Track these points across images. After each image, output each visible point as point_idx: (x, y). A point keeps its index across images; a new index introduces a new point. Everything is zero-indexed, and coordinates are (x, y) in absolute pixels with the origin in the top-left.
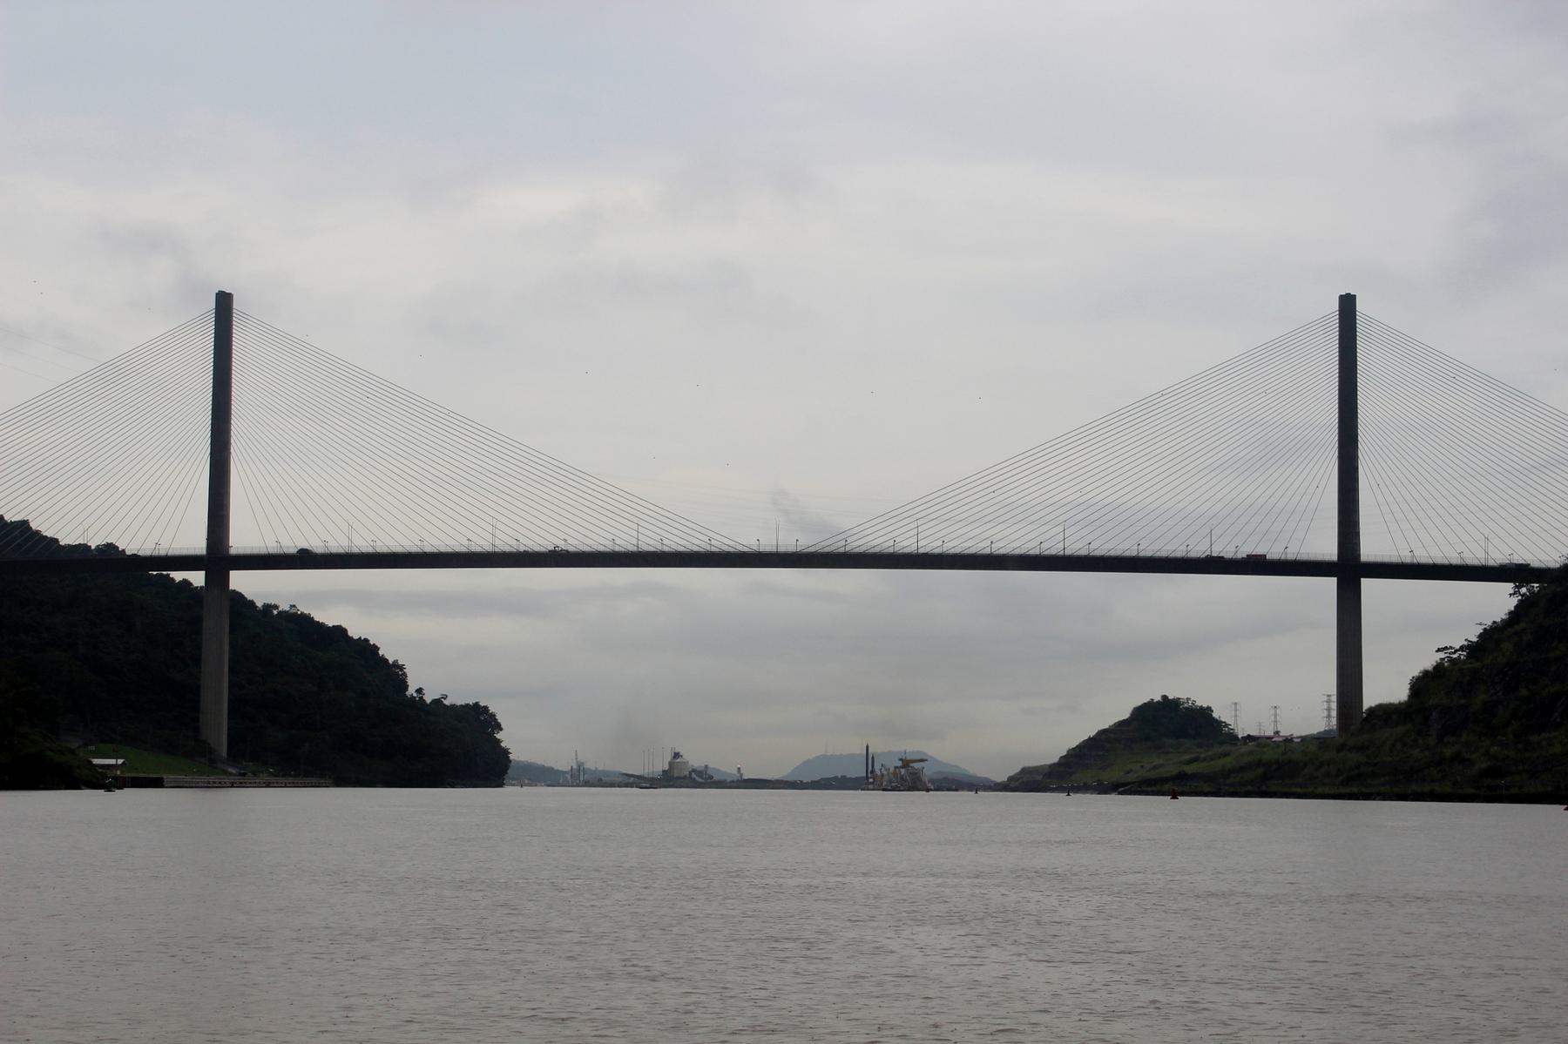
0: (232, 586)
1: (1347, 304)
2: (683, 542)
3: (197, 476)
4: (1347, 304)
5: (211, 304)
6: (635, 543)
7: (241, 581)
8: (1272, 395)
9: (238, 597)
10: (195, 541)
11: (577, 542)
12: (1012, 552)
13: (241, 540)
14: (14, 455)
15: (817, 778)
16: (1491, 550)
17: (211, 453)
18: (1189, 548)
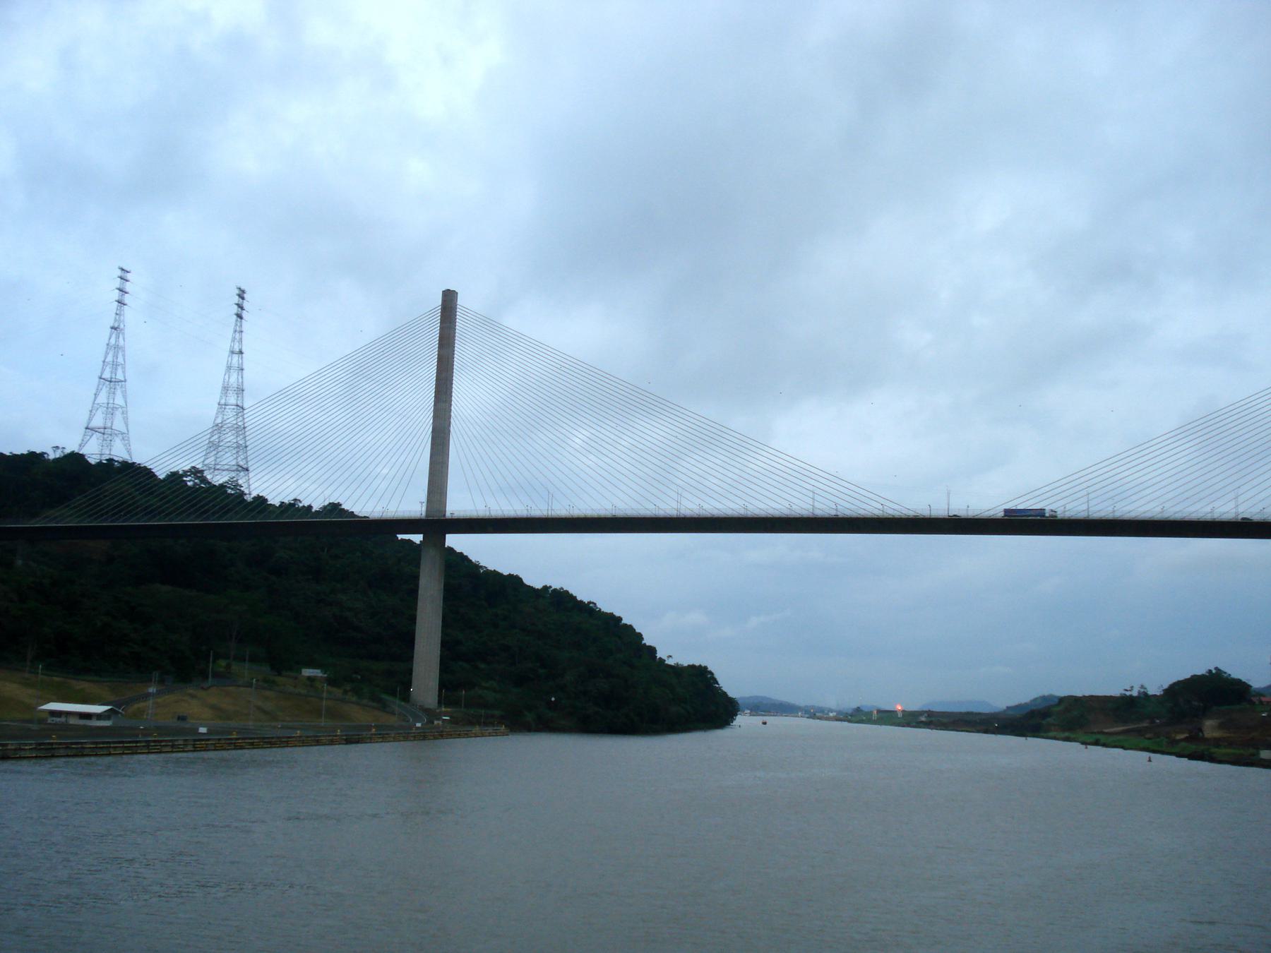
0: (399, 538)
1: (449, 298)
2: (864, 506)
3: (421, 449)
4: (449, 298)
5: (438, 301)
6: (834, 507)
7: (456, 541)
8: (562, 373)
9: (451, 550)
10: (413, 505)
11: (781, 506)
12: (1205, 517)
13: (458, 504)
14: (1241, 433)
15: (914, 706)
16: (685, 502)
17: (432, 432)
18: (1115, 509)
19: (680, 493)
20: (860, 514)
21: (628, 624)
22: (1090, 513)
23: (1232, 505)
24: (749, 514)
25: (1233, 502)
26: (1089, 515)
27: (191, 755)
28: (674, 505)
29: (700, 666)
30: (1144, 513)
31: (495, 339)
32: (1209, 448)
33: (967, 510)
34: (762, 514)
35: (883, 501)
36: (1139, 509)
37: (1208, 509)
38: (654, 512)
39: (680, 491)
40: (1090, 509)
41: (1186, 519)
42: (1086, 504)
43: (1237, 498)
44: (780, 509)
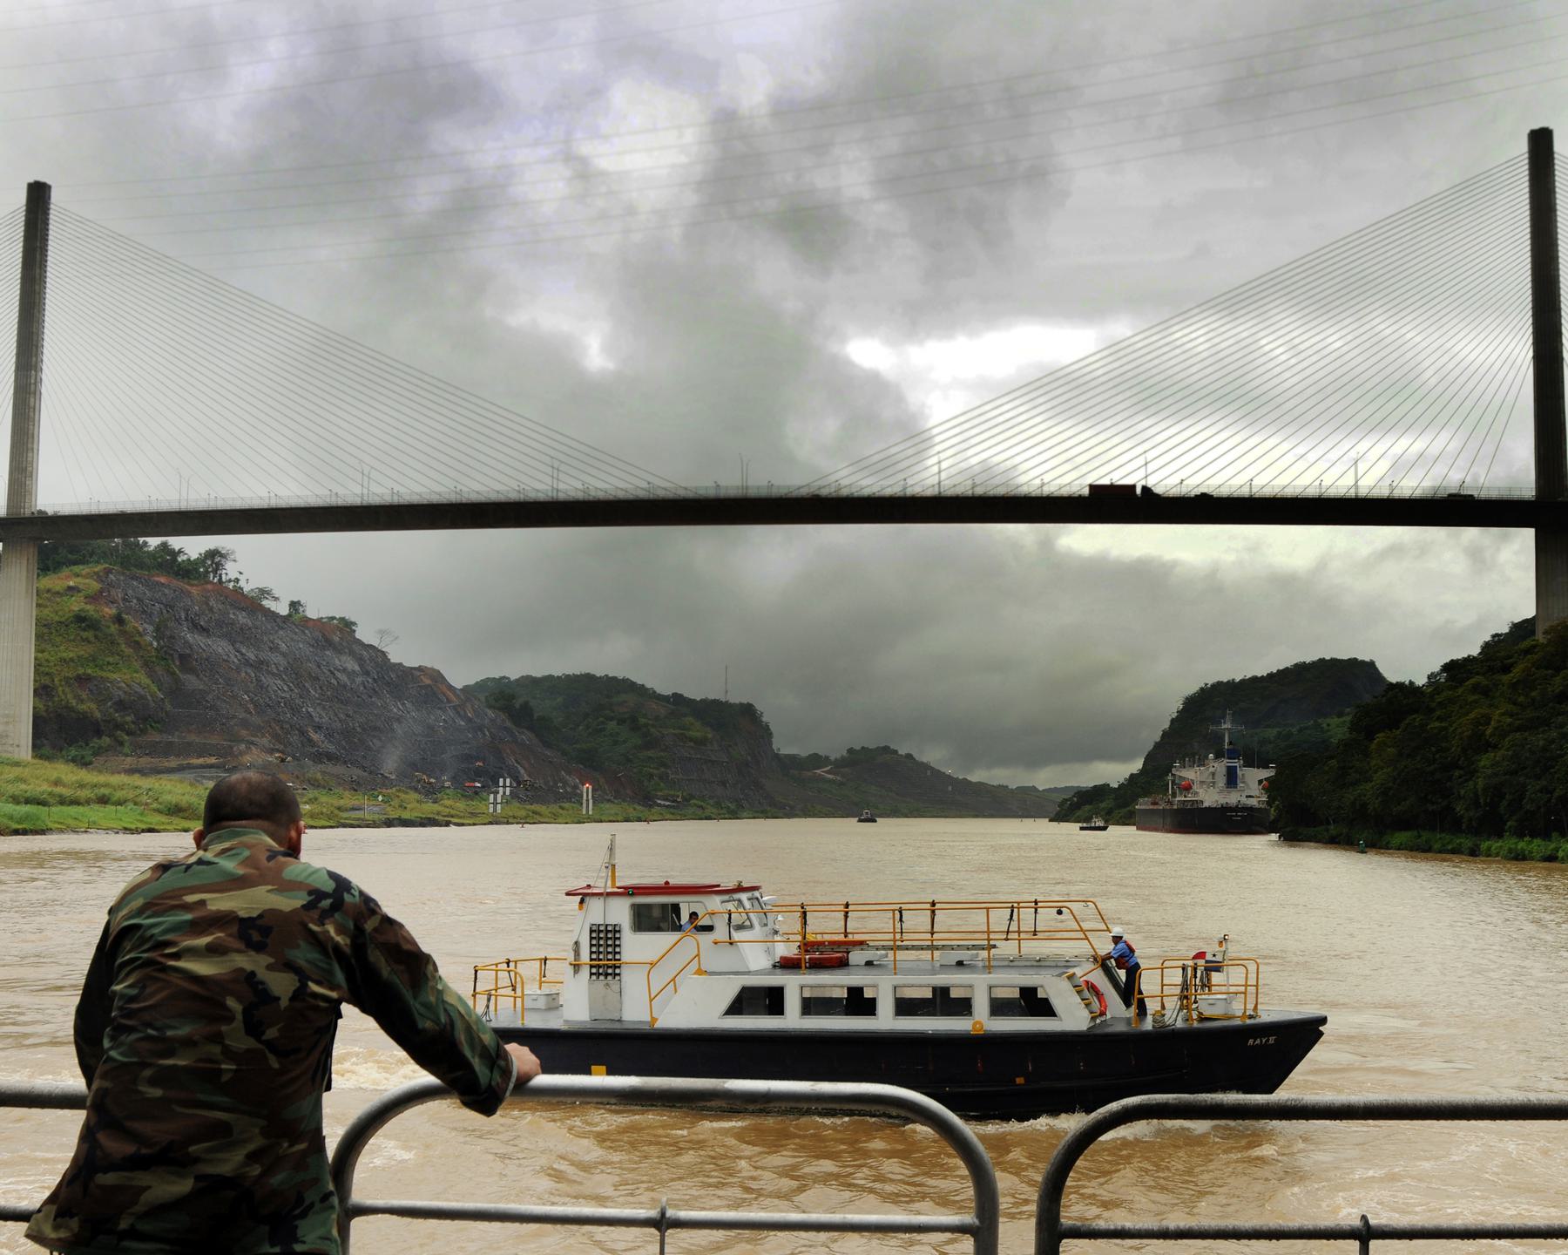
19: (556, 466)
20: (658, 496)
21: (1448, 661)
22: (942, 490)
23: (1141, 473)
24: (340, 502)
25: (365, 477)
26: (940, 493)
27: (32, 678)
28: (358, 490)
29: (477, 683)
30: (799, 488)
31: (245, 331)
32: (1390, 305)
33: (150, 502)
34: (238, 504)
35: (651, 478)
36: (815, 484)
37: (1175, 480)
38: (550, 494)
39: (556, 464)
40: (942, 483)
41: (1235, 495)
42: (937, 477)
43: (939, 462)
44: (566, 490)
